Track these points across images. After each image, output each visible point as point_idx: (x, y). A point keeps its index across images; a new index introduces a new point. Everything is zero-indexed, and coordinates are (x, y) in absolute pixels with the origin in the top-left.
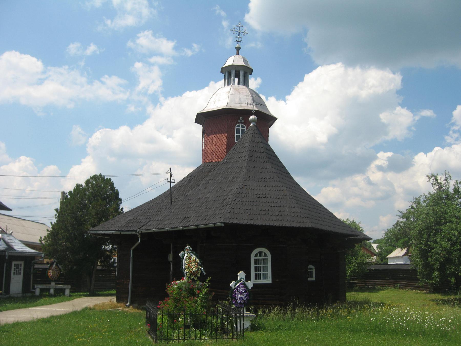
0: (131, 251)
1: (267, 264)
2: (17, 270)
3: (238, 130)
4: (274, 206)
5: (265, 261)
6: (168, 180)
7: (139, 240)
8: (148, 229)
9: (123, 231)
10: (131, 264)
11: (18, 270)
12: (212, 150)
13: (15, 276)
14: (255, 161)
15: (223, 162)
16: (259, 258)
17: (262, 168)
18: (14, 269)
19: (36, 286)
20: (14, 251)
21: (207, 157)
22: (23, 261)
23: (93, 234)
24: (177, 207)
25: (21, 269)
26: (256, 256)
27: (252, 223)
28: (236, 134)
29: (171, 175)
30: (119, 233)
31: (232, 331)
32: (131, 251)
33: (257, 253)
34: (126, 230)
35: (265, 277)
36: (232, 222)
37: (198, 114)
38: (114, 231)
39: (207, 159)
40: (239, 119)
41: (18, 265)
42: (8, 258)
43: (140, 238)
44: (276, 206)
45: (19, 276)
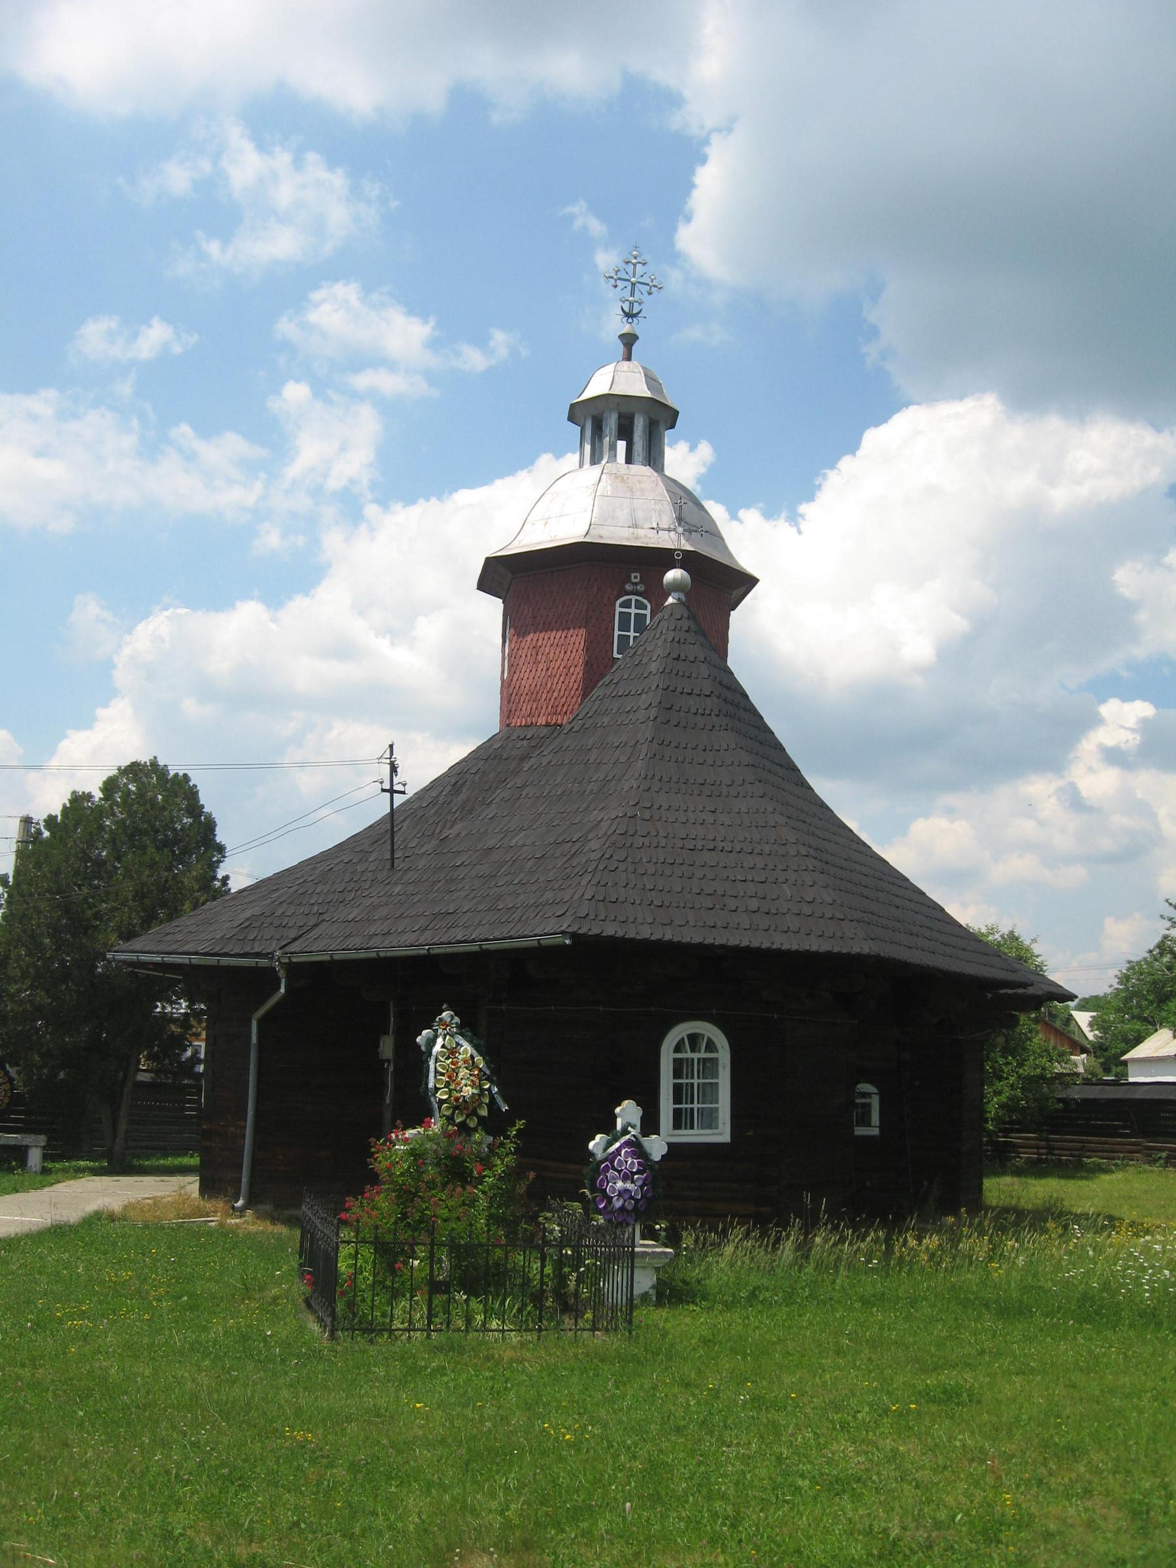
0: (254, 1024)
3: (625, 617)
6: (381, 783)
8: (313, 949)
9: (226, 955)
10: (252, 1066)
16: (689, 1055)
21: (519, 709)
23: (125, 962)
26: (678, 1048)
28: (617, 633)
29: (394, 769)
32: (254, 1024)
33: (683, 1038)
34: (236, 951)
37: (488, 560)
40: (628, 580)
43: (283, 981)
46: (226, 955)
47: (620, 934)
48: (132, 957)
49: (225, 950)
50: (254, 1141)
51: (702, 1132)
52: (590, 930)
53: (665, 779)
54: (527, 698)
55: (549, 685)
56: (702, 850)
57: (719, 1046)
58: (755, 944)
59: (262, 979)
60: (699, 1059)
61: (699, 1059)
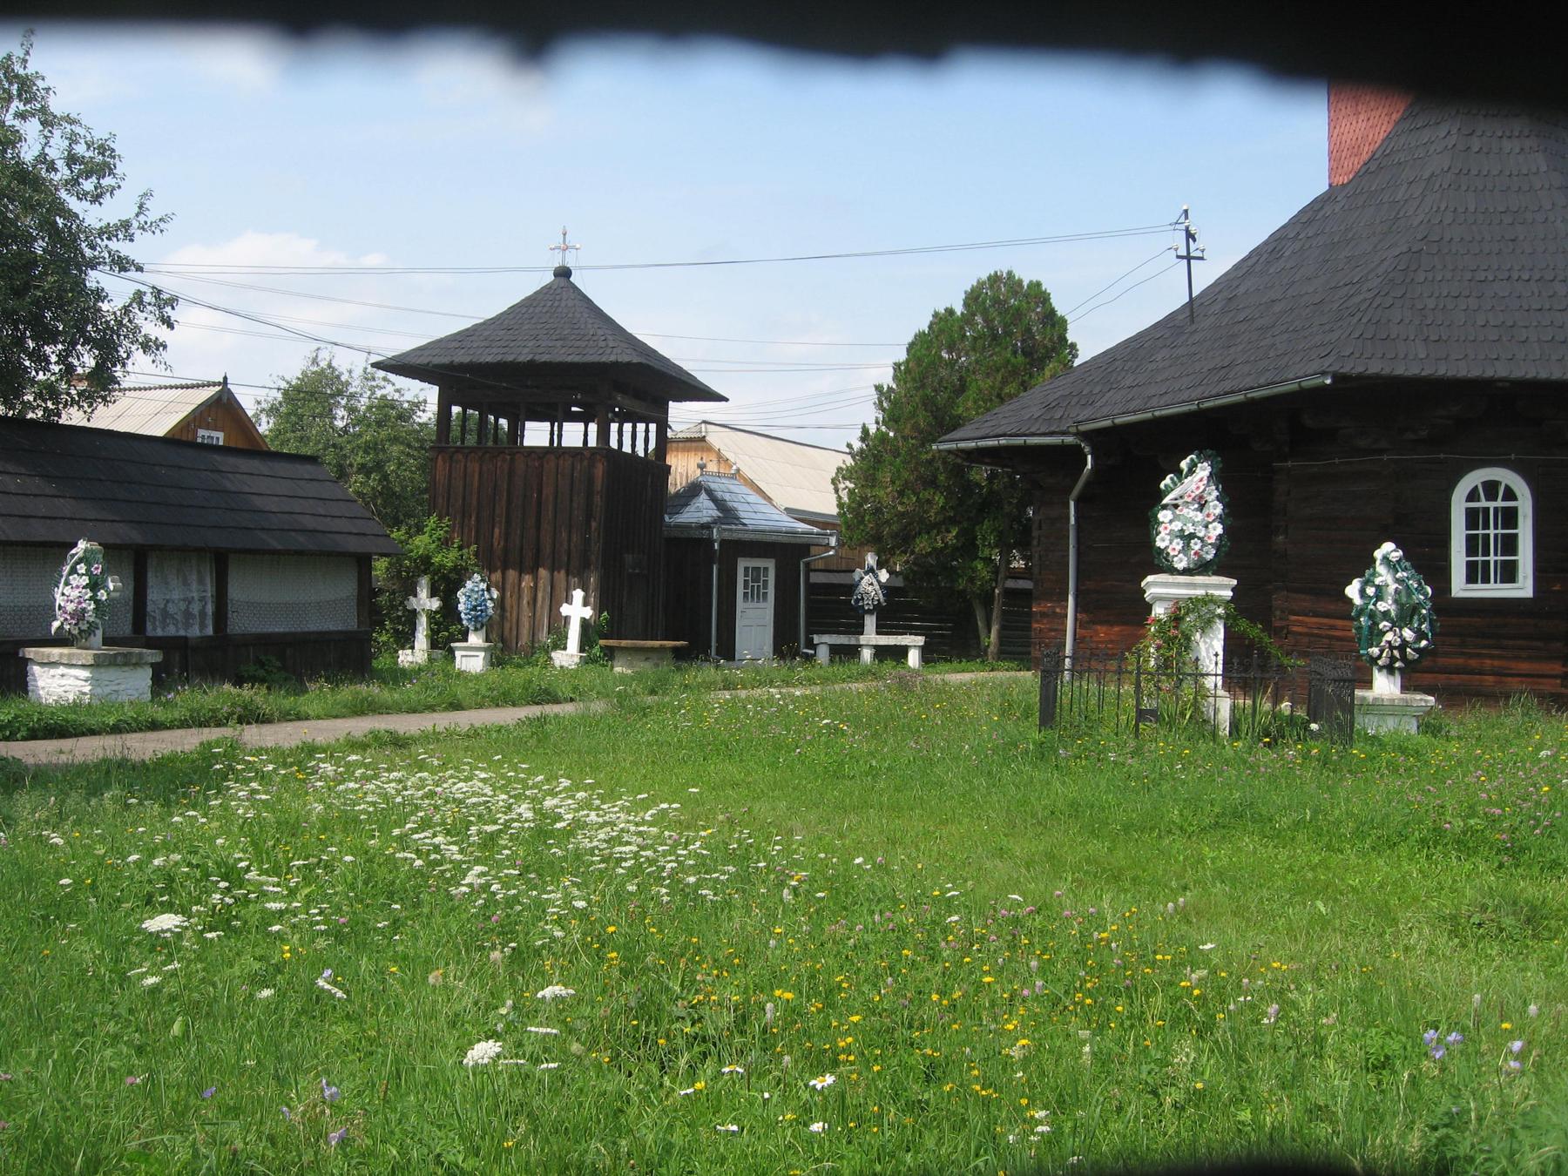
0: (1072, 504)
1: (1515, 527)
2: (753, 586)
4: (1540, 310)
5: (1510, 517)
6: (1176, 250)
7: (1086, 465)
8: (1098, 416)
9: (1033, 435)
10: (1071, 546)
11: (758, 586)
12: (1354, 139)
13: (750, 604)
14: (1485, 150)
15: (1367, 166)
16: (1483, 503)
17: (1508, 173)
18: (765, 587)
19: (816, 639)
20: (740, 527)
21: (1340, 167)
22: (773, 561)
23: (949, 452)
24: (1197, 337)
25: (766, 582)
26: (1473, 496)
27: (1441, 372)
29: (1190, 236)
30: (1019, 441)
31: (1056, 630)
32: (1072, 504)
33: (1477, 486)
34: (1042, 430)
35: (1509, 573)
36: (1360, 369)
38: (1004, 435)
39: (1339, 171)
41: (757, 569)
42: (721, 545)
43: (1089, 457)
44: (1548, 307)
45: (762, 605)
46: (751, 363)
47: (1387, 371)
48: (953, 446)
49: (1033, 430)
50: (1076, 619)
51: (1499, 585)
52: (1353, 368)
53: (1461, 210)
54: (1349, 153)
55: (1371, 136)
56: (1494, 280)
57: (1518, 494)
58: (1543, 375)
59: (1067, 458)
60: (1496, 509)
61: (1496, 509)
